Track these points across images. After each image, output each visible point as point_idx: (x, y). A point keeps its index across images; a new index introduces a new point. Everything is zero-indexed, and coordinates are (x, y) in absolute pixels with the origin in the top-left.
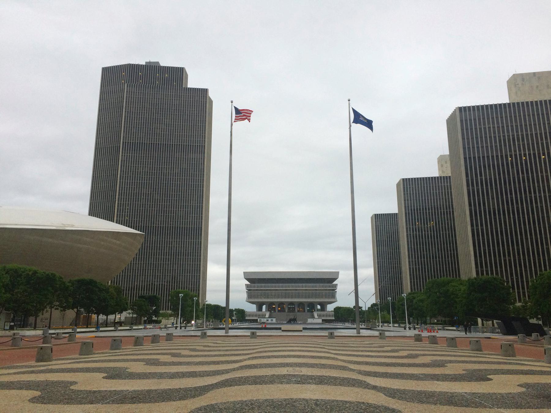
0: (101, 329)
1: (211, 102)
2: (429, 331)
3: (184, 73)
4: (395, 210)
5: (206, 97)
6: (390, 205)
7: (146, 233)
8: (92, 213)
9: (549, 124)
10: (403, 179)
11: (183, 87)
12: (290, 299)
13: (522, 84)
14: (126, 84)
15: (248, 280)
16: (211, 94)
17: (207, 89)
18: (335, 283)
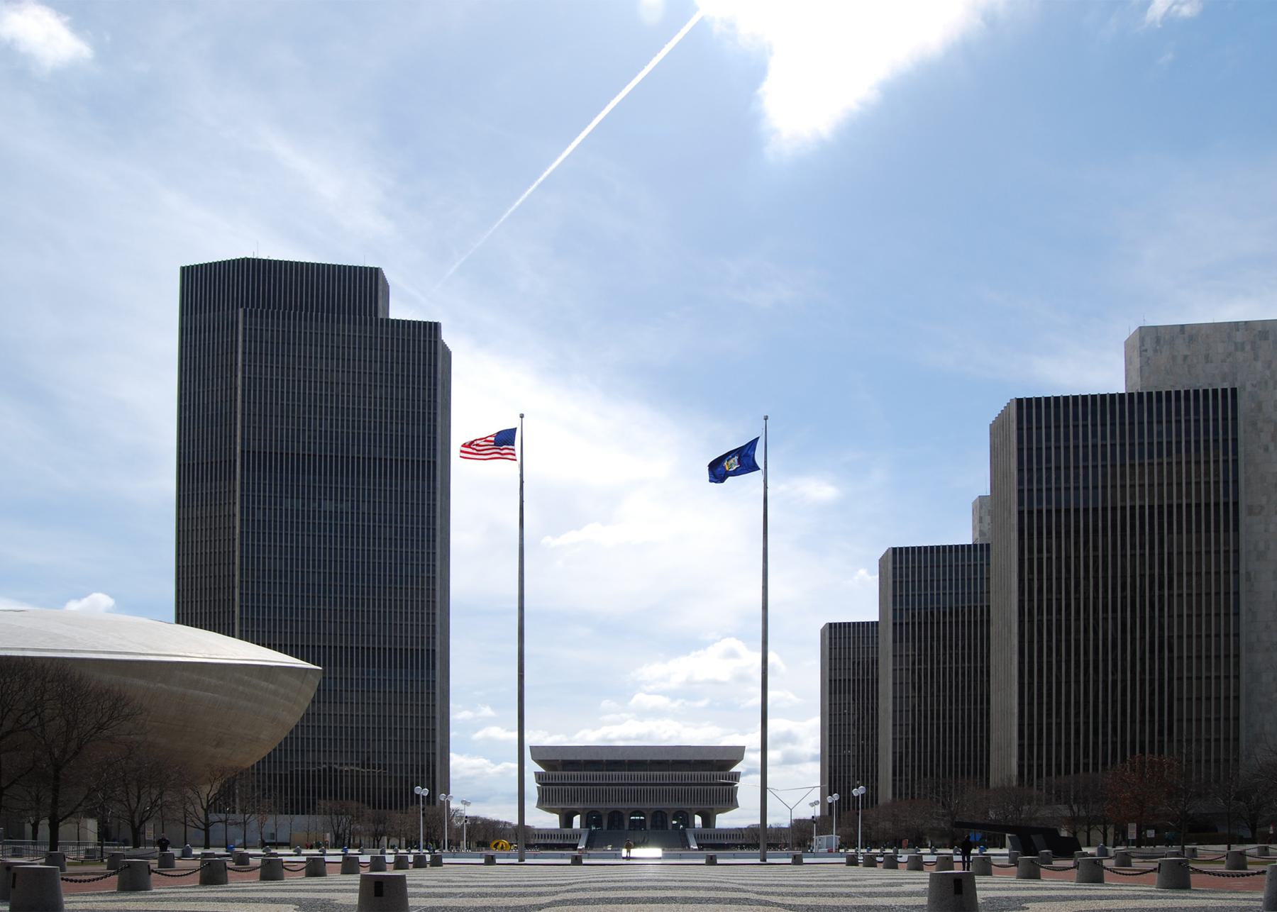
0: (527, 861)
1: (448, 355)
2: (212, 855)
3: (380, 282)
4: (872, 615)
5: (436, 342)
6: (862, 602)
7: (324, 666)
8: (187, 615)
9: (540, 907)
10: (1019, 401)
11: (380, 316)
12: (637, 798)
13: (1155, 351)
14: (241, 311)
15: (540, 762)
16: (446, 337)
17: (436, 324)
18: (734, 769)
